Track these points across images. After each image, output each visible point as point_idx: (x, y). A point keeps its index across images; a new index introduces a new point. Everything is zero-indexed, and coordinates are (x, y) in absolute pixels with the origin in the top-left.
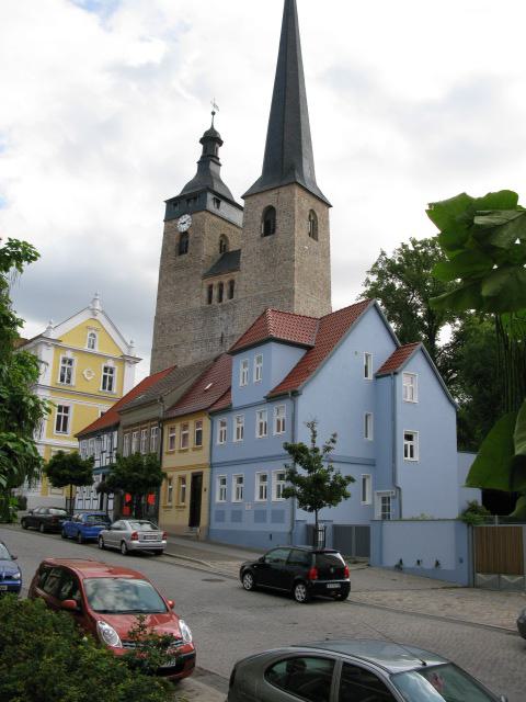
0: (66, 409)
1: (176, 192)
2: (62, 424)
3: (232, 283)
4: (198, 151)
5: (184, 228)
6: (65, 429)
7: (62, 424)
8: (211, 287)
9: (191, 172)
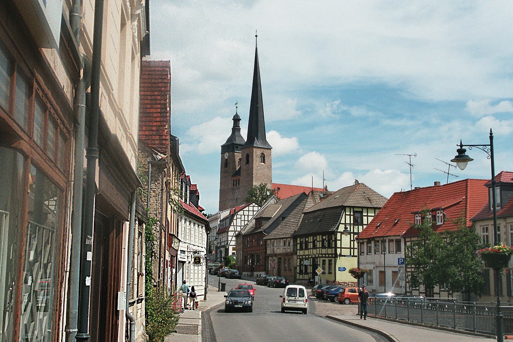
3: (239, 180)
5: (226, 158)
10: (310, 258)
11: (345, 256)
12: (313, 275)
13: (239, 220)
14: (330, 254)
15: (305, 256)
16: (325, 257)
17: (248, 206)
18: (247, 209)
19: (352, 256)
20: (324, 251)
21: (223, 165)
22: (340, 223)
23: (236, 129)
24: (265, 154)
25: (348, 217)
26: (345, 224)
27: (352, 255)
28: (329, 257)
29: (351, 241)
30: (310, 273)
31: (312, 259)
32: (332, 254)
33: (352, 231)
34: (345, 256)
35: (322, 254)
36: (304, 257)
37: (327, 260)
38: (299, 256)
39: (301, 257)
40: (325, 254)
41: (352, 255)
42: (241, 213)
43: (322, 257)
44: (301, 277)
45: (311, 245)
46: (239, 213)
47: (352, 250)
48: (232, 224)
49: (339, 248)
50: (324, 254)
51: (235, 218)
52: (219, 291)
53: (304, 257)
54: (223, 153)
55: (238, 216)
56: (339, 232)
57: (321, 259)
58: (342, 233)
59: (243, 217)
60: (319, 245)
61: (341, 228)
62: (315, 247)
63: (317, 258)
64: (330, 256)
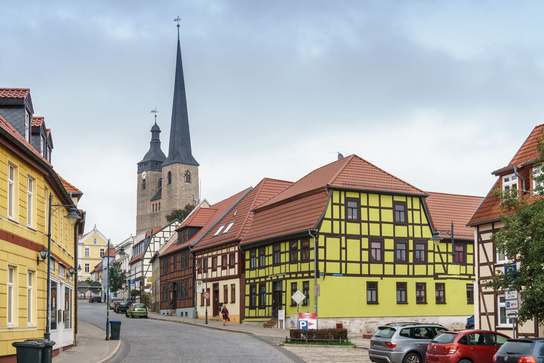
0: (88, 265)
1: (141, 159)
2: (87, 270)
3: (159, 203)
4: (149, 137)
5: (144, 177)
6: (88, 271)
7: (87, 270)
8: (153, 205)
9: (146, 148)
10: (269, 281)
11: (331, 274)
12: (273, 309)
13: (157, 244)
14: (306, 272)
15: (259, 278)
16: (297, 278)
17: (170, 225)
18: (167, 229)
19: (344, 275)
20: (294, 268)
21: (140, 186)
22: (324, 218)
23: (155, 142)
24: (191, 171)
25: (336, 208)
26: (332, 219)
27: (344, 272)
28: (303, 277)
29: (341, 248)
30: (269, 306)
31: (271, 283)
32: (309, 272)
33: (343, 232)
34: (331, 274)
35: (290, 274)
36: (257, 280)
37: (300, 282)
38: (249, 279)
39: (252, 281)
40: (296, 273)
41: (344, 272)
42: (160, 234)
43: (291, 278)
44: (253, 313)
45: (269, 261)
46: (157, 235)
47: (343, 264)
48: (148, 250)
49: (410, 210)
50: (293, 273)
51: (152, 241)
52: (107, 339)
53: (257, 280)
54: (139, 172)
55: (156, 239)
56: (322, 234)
57: (289, 282)
58: (327, 235)
59: (162, 240)
60: (285, 258)
61: (326, 227)
62: (277, 263)
63: (281, 280)
64: (307, 275)
